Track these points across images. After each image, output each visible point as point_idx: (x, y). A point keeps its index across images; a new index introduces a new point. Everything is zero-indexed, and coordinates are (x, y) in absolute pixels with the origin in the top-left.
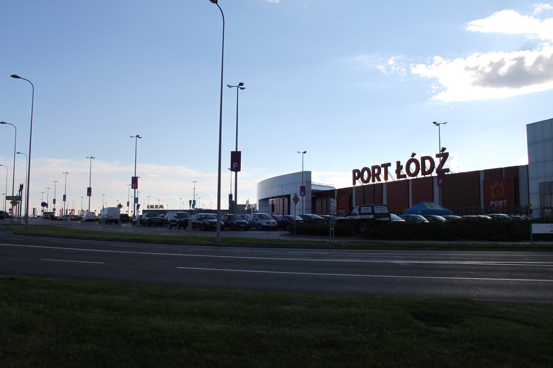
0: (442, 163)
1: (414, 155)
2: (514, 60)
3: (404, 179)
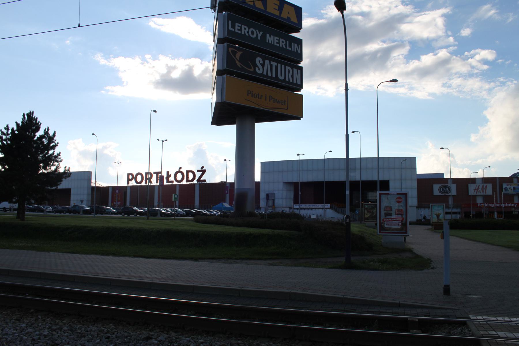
0: (201, 176)
1: (180, 168)
2: (186, 65)
3: (172, 184)
